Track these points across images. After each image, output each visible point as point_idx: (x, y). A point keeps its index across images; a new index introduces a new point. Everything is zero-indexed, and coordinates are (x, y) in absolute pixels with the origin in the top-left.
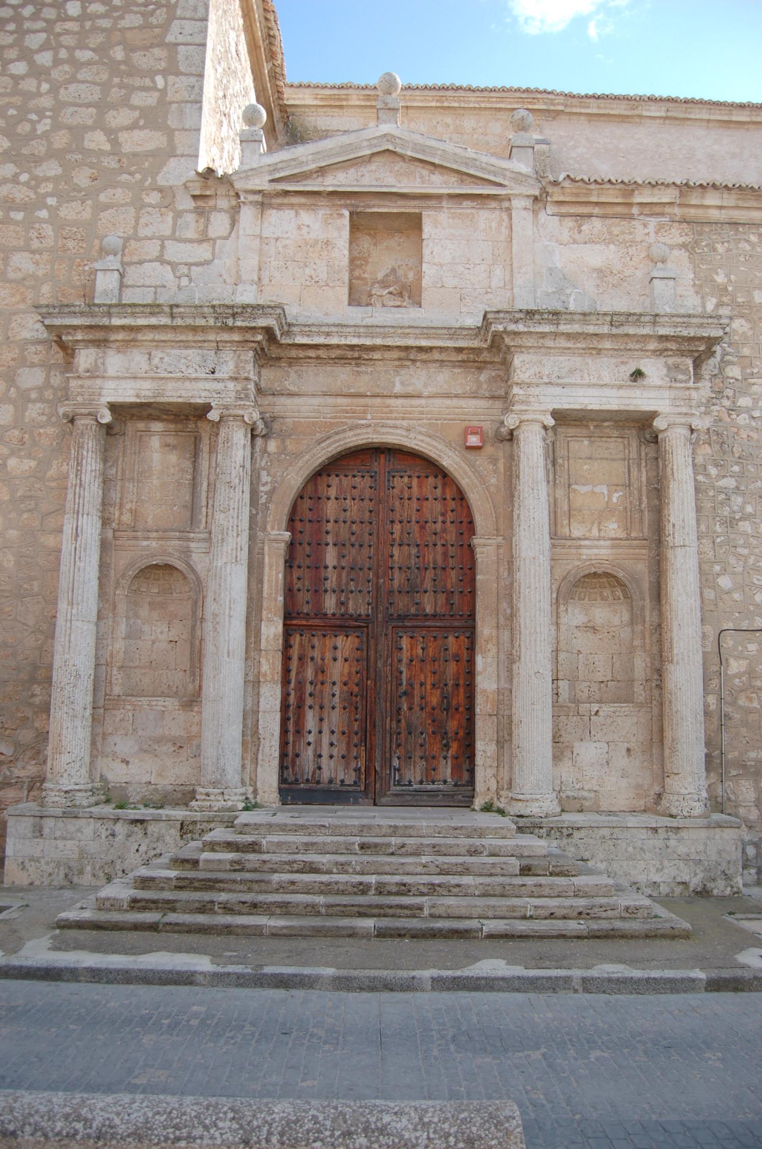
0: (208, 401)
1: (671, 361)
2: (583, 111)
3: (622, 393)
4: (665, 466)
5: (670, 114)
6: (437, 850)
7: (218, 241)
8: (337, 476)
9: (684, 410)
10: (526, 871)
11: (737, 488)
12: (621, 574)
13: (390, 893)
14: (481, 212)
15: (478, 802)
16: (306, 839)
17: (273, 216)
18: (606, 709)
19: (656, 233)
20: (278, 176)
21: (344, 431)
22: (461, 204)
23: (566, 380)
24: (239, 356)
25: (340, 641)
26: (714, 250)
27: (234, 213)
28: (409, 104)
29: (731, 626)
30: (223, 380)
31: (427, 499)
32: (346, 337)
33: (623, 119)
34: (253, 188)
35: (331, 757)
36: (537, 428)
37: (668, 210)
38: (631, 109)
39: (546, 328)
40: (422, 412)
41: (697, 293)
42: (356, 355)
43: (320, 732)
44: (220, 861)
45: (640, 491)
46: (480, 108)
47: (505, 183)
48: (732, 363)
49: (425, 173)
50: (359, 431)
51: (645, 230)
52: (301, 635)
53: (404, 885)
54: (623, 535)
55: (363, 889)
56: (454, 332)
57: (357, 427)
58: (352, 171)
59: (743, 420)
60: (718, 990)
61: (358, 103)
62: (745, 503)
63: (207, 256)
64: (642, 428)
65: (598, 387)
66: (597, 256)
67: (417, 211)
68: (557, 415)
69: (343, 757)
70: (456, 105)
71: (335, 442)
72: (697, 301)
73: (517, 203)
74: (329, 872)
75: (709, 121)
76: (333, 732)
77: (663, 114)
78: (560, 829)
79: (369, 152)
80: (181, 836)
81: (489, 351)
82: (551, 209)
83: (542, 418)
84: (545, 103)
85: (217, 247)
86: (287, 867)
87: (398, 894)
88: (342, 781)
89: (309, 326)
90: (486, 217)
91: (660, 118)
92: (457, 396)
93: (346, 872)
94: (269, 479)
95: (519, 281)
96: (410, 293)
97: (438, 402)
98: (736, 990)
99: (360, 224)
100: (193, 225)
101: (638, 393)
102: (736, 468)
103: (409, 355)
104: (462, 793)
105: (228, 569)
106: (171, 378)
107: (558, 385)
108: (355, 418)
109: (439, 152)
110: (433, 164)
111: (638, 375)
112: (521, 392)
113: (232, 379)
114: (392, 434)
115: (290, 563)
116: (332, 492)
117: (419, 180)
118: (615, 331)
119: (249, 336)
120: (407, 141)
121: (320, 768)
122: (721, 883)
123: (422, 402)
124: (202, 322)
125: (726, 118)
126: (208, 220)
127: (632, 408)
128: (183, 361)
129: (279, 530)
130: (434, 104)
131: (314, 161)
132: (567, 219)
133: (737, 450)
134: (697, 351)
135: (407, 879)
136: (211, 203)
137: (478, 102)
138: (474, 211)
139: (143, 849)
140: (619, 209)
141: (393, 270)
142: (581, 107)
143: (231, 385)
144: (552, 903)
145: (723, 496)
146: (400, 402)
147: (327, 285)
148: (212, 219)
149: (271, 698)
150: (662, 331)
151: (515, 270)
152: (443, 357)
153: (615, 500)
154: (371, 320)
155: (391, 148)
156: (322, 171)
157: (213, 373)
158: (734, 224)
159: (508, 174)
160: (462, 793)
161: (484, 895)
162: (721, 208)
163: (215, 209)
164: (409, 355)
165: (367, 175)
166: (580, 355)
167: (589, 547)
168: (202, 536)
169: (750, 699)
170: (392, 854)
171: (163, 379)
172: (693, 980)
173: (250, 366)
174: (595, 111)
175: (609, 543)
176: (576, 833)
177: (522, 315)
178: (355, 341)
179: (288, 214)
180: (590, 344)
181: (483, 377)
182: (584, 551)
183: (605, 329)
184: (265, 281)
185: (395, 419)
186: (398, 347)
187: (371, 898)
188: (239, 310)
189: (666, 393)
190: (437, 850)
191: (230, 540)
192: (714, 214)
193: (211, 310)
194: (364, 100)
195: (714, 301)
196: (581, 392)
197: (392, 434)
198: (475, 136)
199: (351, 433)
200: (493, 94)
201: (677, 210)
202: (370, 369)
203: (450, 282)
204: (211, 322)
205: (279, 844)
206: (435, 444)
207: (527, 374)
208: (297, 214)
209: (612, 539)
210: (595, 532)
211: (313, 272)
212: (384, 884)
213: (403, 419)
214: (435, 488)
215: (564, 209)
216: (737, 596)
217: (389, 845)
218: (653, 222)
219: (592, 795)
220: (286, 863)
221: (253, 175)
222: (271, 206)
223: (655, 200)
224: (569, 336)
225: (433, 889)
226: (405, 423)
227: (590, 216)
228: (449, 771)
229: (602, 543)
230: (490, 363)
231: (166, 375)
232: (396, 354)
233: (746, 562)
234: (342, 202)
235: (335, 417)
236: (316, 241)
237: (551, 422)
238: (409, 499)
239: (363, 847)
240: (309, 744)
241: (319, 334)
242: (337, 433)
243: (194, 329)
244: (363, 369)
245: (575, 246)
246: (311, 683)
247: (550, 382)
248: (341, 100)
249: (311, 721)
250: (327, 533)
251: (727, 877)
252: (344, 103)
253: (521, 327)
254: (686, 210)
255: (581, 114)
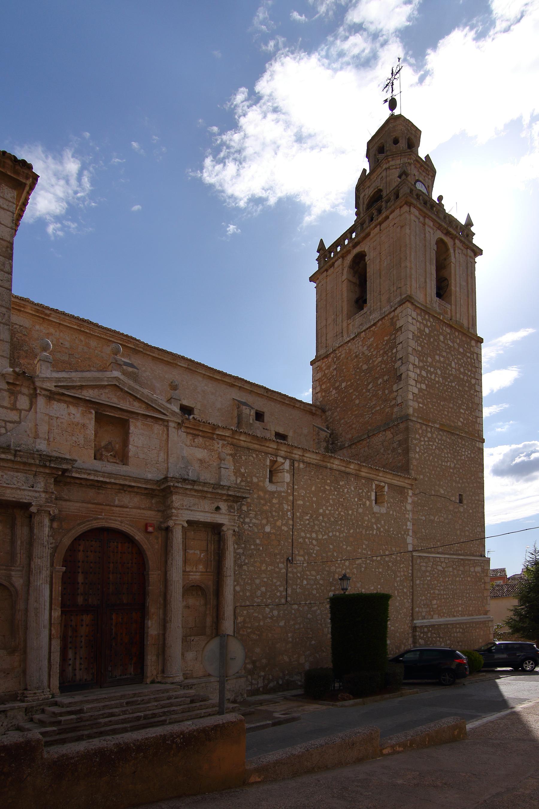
0: (30, 501)
1: (229, 504)
2: (151, 354)
3: (212, 515)
4: (224, 545)
5: (189, 367)
6: (156, 700)
7: (23, 412)
8: (84, 540)
9: (233, 524)
10: (192, 702)
11: (243, 553)
12: (203, 586)
13: (149, 718)
14: (156, 425)
15: (148, 681)
16: (102, 704)
17: (56, 405)
18: (197, 638)
19: (222, 447)
20: (60, 384)
21: (91, 520)
22: (147, 419)
23: (192, 508)
24: (47, 480)
25: (84, 617)
26: (242, 458)
27: (33, 397)
28: (61, 322)
29: (239, 604)
30: (39, 492)
31: (125, 553)
32: (97, 477)
33: (168, 363)
34: (46, 387)
35: (80, 669)
36: (180, 527)
37: (227, 438)
38: (173, 360)
39: (189, 487)
40: (128, 514)
41: (234, 475)
42: (100, 485)
43: (75, 659)
44: (71, 719)
45: (211, 553)
46: (100, 337)
47: (168, 414)
48: (245, 505)
49: (131, 400)
50: (99, 521)
51: (218, 445)
52: (66, 615)
53: (154, 714)
54: (204, 570)
55: (138, 718)
56: (147, 481)
57: (98, 519)
58: (96, 390)
59: (246, 527)
60: (274, 726)
61: (30, 312)
62: (245, 559)
63: (16, 418)
64: (216, 529)
65: (203, 513)
66: (201, 454)
67: (127, 418)
68: (188, 522)
69: (86, 669)
70: (88, 331)
71: (88, 525)
72: (234, 478)
73: (172, 425)
74: (119, 715)
75: (204, 375)
76: (81, 658)
77: (186, 366)
78: (188, 686)
79: (106, 383)
80: (26, 714)
81: (161, 492)
82: (183, 429)
83: (183, 523)
84: (134, 345)
85: (22, 415)
86: (101, 716)
87: (152, 718)
88: (86, 680)
89: (81, 469)
90: (158, 428)
91: (184, 367)
92: (143, 509)
93: (126, 714)
94: (54, 541)
95: (171, 460)
96: (123, 457)
97: (134, 510)
98: (279, 725)
99: (100, 419)
100: (7, 399)
101: (217, 516)
102: (243, 546)
103: (124, 488)
104: (139, 677)
105: (43, 586)
106: (9, 487)
107: (190, 510)
108: (97, 514)
109: (140, 393)
110: (136, 397)
111: (218, 508)
112: (175, 512)
113: (44, 492)
114: (114, 523)
115: (63, 583)
116: (81, 548)
117: (128, 403)
118: (214, 491)
119: (54, 471)
120: (126, 383)
121: (75, 675)
122: (240, 697)
123: (128, 510)
124: (32, 461)
125: (212, 375)
126: (17, 398)
127: (215, 522)
128: (15, 479)
129: (59, 566)
130: (76, 327)
131: (80, 381)
132: (190, 435)
133: (244, 538)
134: (236, 500)
135: (155, 711)
136: (18, 388)
137: (100, 334)
138: (152, 424)
139: (5, 724)
140: (209, 435)
141: (110, 443)
142: (150, 352)
143: (43, 495)
144: (209, 710)
145: (238, 556)
146: (118, 509)
147: (84, 447)
148: (19, 398)
149: (56, 645)
150: (230, 493)
151: (169, 455)
152: (138, 491)
153: (202, 556)
154: (106, 468)
155: (117, 384)
156: (82, 387)
157: (33, 487)
158: (248, 449)
159: (169, 410)
160: (139, 677)
161: (183, 712)
162: (245, 441)
163: (20, 392)
164: (124, 488)
165: (104, 394)
166: (198, 498)
167: (192, 575)
168: (18, 568)
169: (244, 631)
170: (139, 704)
171: (4, 487)
172: (268, 724)
173: (52, 486)
174: (157, 356)
175: (200, 574)
176: (193, 687)
177: (181, 480)
178: (101, 479)
179: (63, 406)
180: (203, 495)
181: (153, 501)
182: (191, 577)
183: (210, 490)
184: (51, 439)
185: (116, 516)
186: (120, 485)
187: (142, 722)
188: (54, 459)
189: (227, 517)
190: (156, 700)
191: (44, 572)
192: (243, 444)
193: (39, 456)
194: (34, 311)
195: (240, 479)
196: (198, 513)
197: (114, 523)
198: (96, 352)
199: (95, 522)
200: (108, 332)
201: (230, 439)
202: (104, 492)
203: (141, 456)
204: (37, 462)
205: (91, 708)
206: (133, 529)
207: (178, 504)
208: (68, 407)
209: (201, 572)
210: (194, 569)
211: (76, 439)
212: (147, 715)
213: (119, 517)
214: (129, 548)
215: (188, 431)
216: (241, 594)
217: (138, 701)
218: (221, 442)
219: (190, 672)
220: (101, 715)
221: (46, 381)
222: (54, 399)
223: (223, 434)
224: (196, 491)
225: (164, 713)
226: (119, 519)
227: (198, 435)
228: (132, 669)
229: (197, 575)
230: (158, 495)
231: (5, 485)
232: (118, 487)
233: (244, 581)
234: (91, 406)
235: (87, 513)
236: (78, 423)
237: (186, 525)
238: (117, 552)
239: (127, 703)
240: (70, 665)
241: (85, 473)
242: (88, 521)
243: (25, 464)
244: (101, 491)
245: (191, 448)
246: (70, 637)
247: (189, 509)
248: (21, 307)
249: (70, 654)
250: (79, 567)
251: (242, 695)
252: (22, 309)
253: (180, 485)
254: (233, 440)
255: (150, 355)
